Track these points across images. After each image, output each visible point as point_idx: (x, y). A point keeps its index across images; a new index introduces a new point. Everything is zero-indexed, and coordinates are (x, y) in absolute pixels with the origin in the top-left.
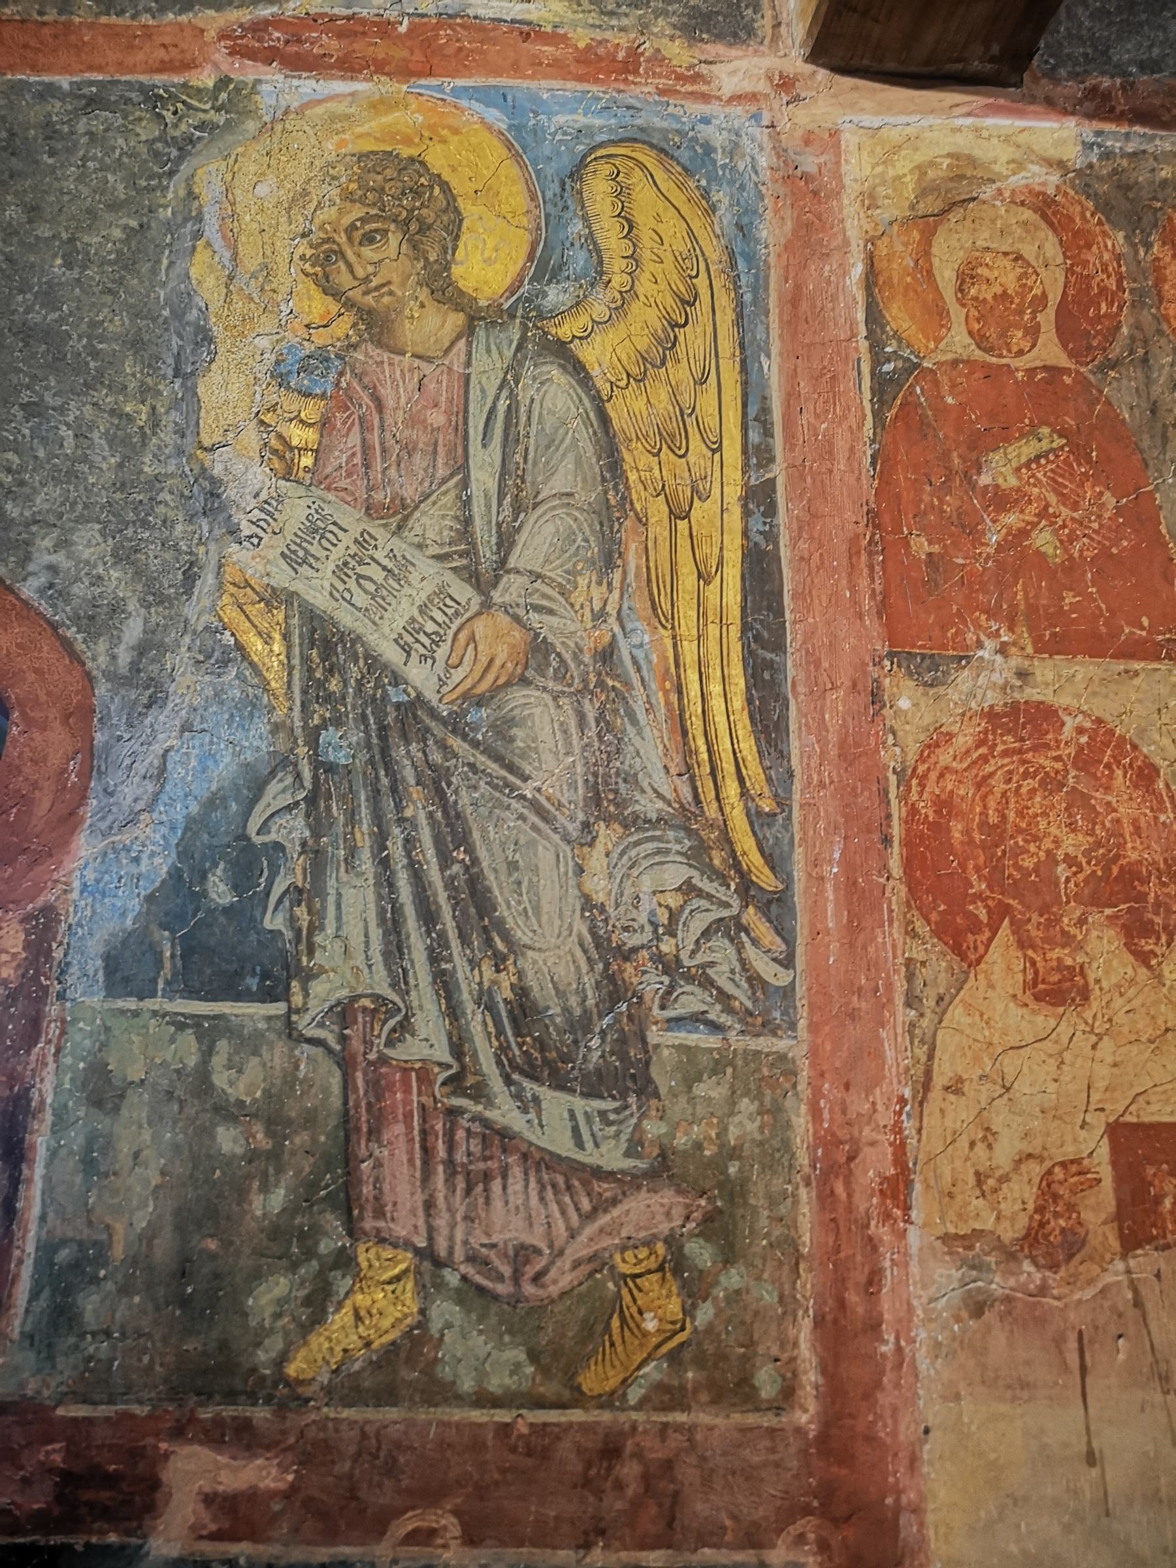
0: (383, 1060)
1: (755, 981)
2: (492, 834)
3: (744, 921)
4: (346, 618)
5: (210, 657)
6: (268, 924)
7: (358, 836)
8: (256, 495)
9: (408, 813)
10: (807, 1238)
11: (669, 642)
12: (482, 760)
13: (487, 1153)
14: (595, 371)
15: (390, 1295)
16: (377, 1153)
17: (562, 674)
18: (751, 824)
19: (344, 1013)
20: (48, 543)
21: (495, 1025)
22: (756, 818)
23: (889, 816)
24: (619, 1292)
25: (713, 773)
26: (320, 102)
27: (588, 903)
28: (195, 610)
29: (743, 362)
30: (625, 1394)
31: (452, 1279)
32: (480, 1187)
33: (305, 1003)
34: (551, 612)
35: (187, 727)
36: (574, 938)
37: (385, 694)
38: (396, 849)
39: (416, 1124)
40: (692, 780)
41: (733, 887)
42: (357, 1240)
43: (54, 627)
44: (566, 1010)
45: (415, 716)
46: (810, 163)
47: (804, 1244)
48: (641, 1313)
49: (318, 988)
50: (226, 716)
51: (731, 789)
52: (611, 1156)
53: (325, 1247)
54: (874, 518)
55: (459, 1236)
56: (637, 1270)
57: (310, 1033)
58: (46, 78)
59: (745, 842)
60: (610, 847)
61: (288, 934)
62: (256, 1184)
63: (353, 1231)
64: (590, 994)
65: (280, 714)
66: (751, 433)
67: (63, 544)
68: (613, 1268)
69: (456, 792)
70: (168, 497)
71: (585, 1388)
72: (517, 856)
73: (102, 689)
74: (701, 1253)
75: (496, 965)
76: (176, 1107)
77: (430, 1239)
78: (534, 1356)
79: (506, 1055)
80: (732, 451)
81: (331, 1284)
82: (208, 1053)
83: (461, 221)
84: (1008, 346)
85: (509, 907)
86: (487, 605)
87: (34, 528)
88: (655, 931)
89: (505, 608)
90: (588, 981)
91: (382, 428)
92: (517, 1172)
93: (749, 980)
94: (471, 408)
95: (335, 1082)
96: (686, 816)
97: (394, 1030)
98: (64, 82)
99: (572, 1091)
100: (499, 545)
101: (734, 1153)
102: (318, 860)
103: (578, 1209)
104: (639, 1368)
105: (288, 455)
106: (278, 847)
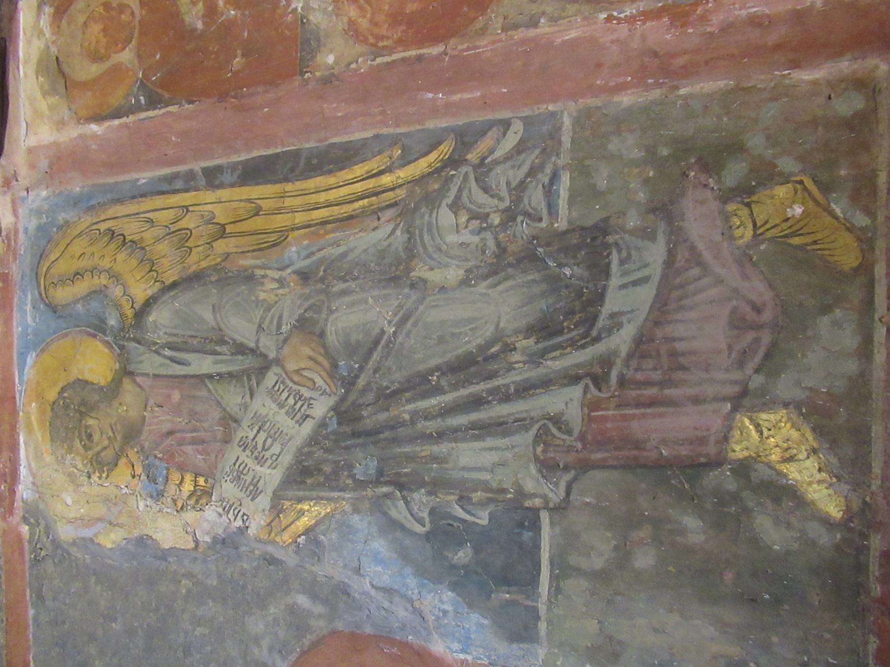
0: (582, 438)
1: (520, 148)
2: (420, 356)
3: (477, 162)
4: (287, 459)
5: (315, 552)
6: (485, 522)
7: (423, 454)
8: (220, 515)
9: (407, 417)
10: (721, 84)
11: (297, 233)
12: (371, 365)
13: (654, 354)
14: (150, 292)
15: (771, 433)
16: (654, 443)
17: (315, 308)
18: (409, 163)
19: (548, 467)
20: (256, 651)
21: (555, 350)
22: (406, 160)
23: (403, 60)
24: (769, 240)
25: (376, 194)
26: (30, 465)
27: (465, 282)
28: (291, 560)
29: (142, 196)
30: (861, 229)
31: (757, 381)
32: (683, 360)
33: (541, 496)
34: (280, 317)
35: (358, 571)
36: (490, 291)
37: (334, 433)
38: (431, 426)
39: (631, 412)
40: (382, 209)
41: (453, 172)
42: (725, 459)
43: (304, 653)
44: (543, 295)
45: (345, 412)
46: (44, 164)
47: (726, 85)
48: (787, 220)
49: (529, 486)
50: (349, 544)
51: (387, 180)
52: (655, 253)
53: (731, 485)
54: (223, 97)
55: (721, 376)
56: (751, 226)
57: (562, 493)
58: (31, 622)
59: (422, 166)
60: (426, 267)
61: (492, 508)
62: (679, 539)
63: (718, 462)
64: (530, 278)
65: (348, 508)
66: (177, 188)
67: (257, 641)
68: (748, 246)
69: (392, 382)
70: (229, 570)
71: (855, 264)
72: (434, 336)
73: (340, 625)
74: (735, 171)
75: (511, 351)
76: (619, 598)
77: (724, 399)
78: (826, 309)
79: (578, 341)
80: (187, 198)
81: (762, 481)
82: (579, 571)
83: (79, 380)
84: (130, 23)
85: (469, 342)
86: (278, 362)
87: (249, 659)
88: (485, 229)
89: (279, 349)
90: (522, 278)
91: (183, 431)
92: (669, 330)
93: (519, 152)
94: (170, 373)
95: (598, 475)
96: (405, 211)
97: (559, 429)
98: (31, 612)
99: (605, 288)
100: (243, 354)
101: (651, 151)
102: (436, 486)
103: (700, 278)
104: (837, 218)
105: (199, 493)
106: (432, 512)
